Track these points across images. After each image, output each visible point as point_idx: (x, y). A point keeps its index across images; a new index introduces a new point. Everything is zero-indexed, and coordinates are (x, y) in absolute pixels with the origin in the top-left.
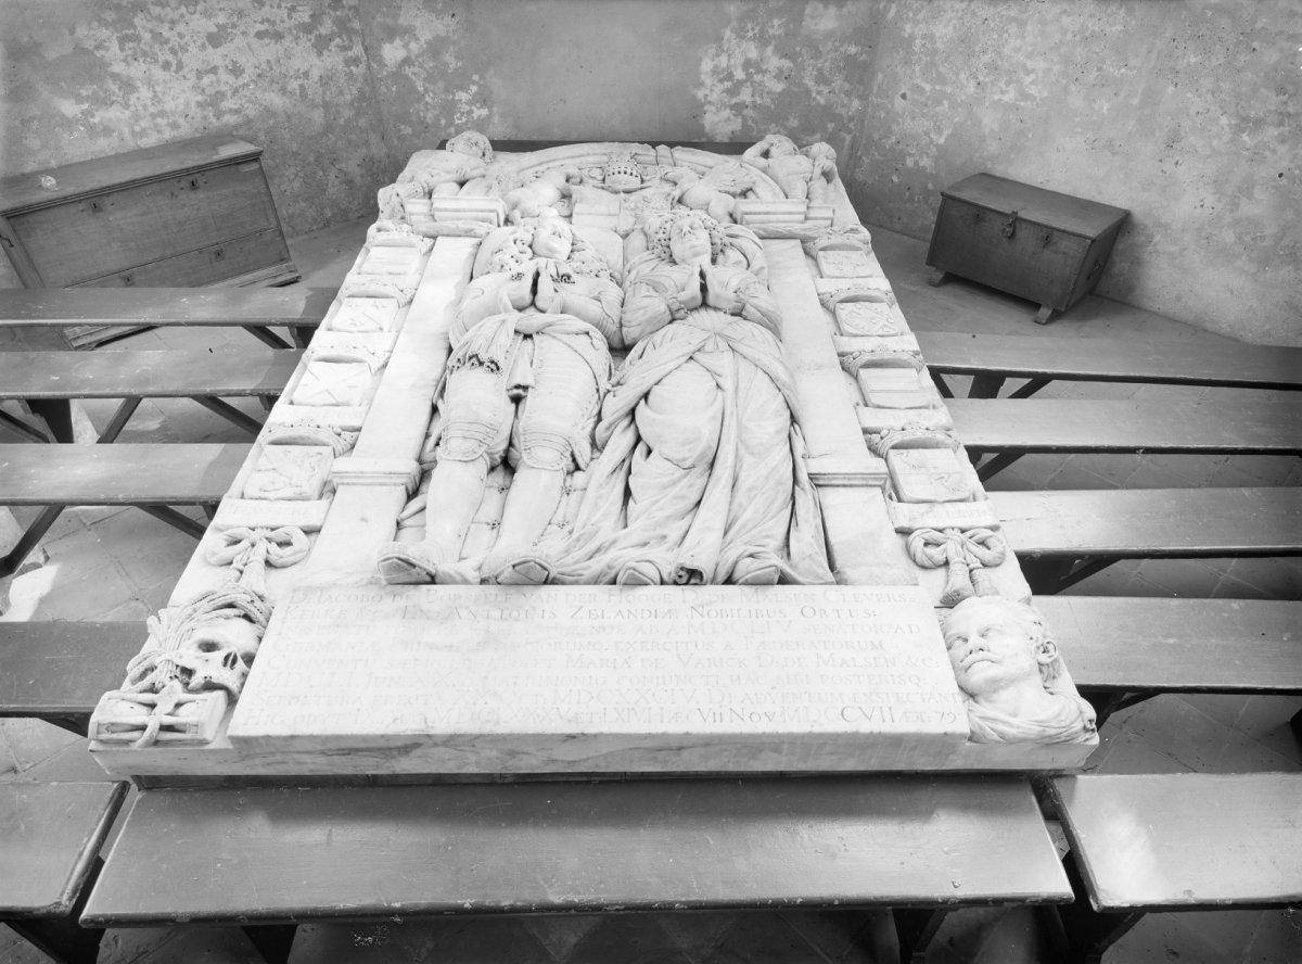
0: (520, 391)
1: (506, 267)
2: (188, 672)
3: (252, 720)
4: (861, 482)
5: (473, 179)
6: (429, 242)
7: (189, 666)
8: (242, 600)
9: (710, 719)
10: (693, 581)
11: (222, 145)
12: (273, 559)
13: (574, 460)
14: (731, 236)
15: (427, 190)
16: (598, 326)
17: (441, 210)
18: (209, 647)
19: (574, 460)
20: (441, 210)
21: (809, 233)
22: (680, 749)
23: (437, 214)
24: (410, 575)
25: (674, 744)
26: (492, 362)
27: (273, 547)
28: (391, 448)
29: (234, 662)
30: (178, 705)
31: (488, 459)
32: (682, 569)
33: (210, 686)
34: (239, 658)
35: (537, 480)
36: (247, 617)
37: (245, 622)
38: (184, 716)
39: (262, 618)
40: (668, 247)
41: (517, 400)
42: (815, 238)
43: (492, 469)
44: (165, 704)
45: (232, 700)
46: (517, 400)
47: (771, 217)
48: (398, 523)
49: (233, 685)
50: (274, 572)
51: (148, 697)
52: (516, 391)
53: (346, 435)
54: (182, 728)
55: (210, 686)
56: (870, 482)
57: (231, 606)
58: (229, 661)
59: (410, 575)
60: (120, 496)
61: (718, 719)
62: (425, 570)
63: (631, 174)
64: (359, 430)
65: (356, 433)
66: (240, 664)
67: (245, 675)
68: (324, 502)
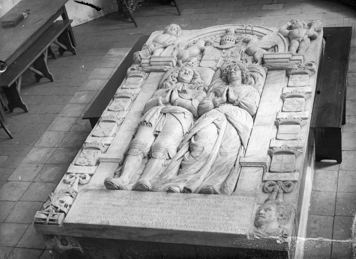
0: (157, 133)
2: (57, 208)
3: (70, 219)
4: (249, 165)
5: (169, 46)
7: (57, 206)
8: (71, 192)
9: (179, 227)
10: (188, 192)
11: (87, 23)
12: (81, 182)
13: (169, 156)
14: (252, 71)
15: (151, 52)
16: (189, 110)
17: (153, 62)
18: (62, 202)
19: (169, 156)
20: (153, 62)
21: (289, 67)
22: (172, 235)
23: (152, 63)
27: (81, 179)
28: (116, 152)
29: (67, 206)
30: (54, 215)
31: (142, 155)
34: (68, 206)
36: (71, 196)
37: (71, 198)
38: (56, 217)
39: (74, 197)
40: (227, 77)
41: (156, 136)
42: (291, 69)
43: (145, 157)
46: (156, 136)
47: (276, 60)
48: (115, 173)
50: (80, 186)
51: (47, 213)
52: (156, 133)
53: (106, 147)
54: (54, 220)
55: (61, 211)
56: (252, 165)
57: (68, 193)
61: (181, 227)
62: (116, 185)
63: (230, 40)
64: (109, 145)
65: (109, 146)
66: (68, 207)
68: (96, 167)
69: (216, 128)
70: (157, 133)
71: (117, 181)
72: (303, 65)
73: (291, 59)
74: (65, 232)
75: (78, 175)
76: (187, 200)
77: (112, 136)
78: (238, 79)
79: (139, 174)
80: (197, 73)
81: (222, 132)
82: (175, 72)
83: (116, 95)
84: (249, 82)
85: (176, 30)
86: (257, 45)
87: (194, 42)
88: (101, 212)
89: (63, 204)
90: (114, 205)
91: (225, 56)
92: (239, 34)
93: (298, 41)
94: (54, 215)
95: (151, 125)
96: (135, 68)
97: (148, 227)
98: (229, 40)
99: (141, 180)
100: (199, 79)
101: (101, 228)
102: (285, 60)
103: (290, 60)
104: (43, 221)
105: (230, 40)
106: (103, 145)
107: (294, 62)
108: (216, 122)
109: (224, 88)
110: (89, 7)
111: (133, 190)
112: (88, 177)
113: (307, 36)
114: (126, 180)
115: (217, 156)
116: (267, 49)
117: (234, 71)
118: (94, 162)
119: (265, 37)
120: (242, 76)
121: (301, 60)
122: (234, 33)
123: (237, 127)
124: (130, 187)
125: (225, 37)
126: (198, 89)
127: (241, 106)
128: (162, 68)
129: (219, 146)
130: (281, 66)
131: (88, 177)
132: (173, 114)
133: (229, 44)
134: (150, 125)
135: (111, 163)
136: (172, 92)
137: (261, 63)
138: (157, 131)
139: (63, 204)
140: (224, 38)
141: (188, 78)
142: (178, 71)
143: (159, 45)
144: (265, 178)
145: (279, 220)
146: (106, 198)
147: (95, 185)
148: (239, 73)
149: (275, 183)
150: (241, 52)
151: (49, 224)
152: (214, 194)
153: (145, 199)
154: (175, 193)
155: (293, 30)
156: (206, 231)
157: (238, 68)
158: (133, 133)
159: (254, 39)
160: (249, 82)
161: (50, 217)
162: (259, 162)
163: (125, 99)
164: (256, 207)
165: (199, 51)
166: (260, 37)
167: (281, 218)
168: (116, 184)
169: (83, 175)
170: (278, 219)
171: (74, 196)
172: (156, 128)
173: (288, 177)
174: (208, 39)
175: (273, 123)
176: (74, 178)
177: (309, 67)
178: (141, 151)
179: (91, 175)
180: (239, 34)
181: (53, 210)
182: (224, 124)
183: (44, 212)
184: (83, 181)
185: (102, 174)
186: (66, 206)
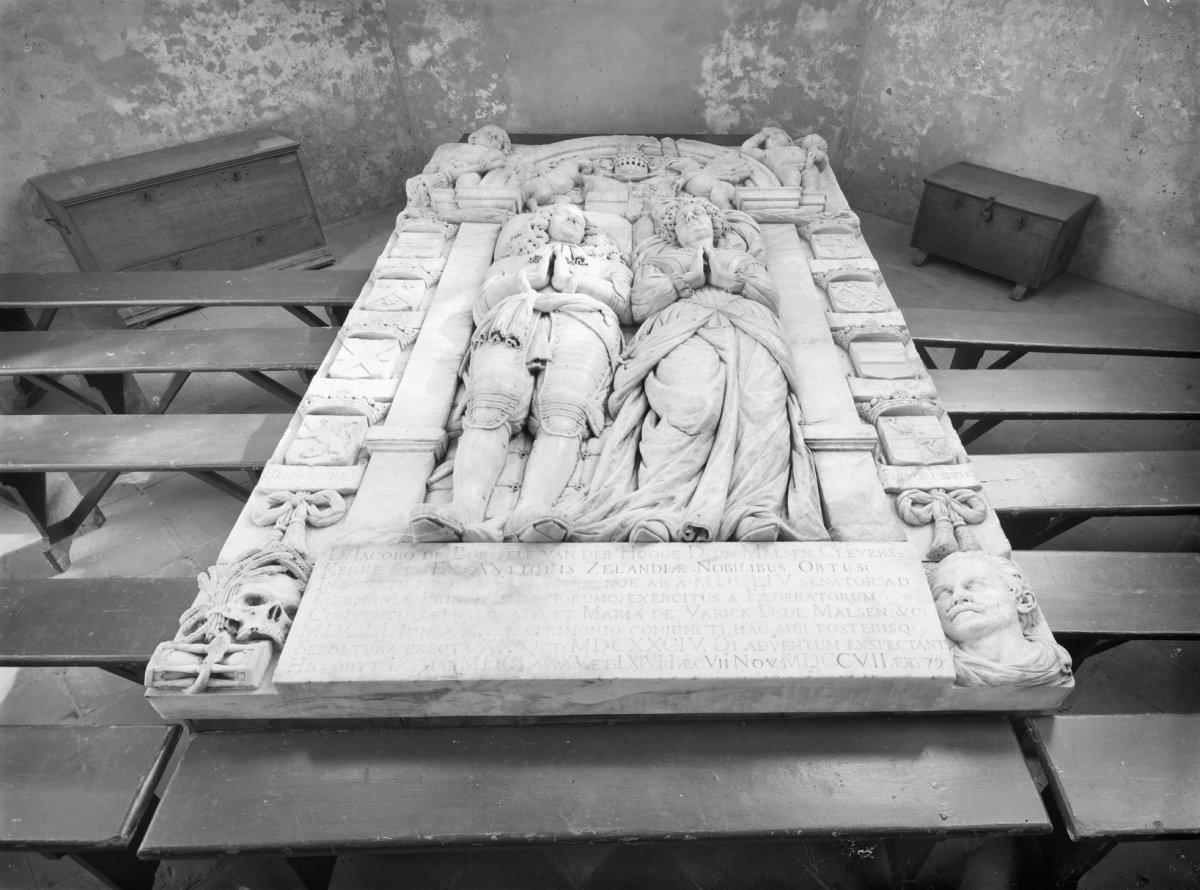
2: (236, 624)
3: (295, 667)
4: (852, 447)
5: (493, 169)
8: (285, 557)
10: (699, 538)
12: (313, 519)
22: (688, 693)
24: (439, 534)
25: (683, 688)
26: (513, 338)
27: (313, 509)
29: (279, 614)
30: (227, 654)
31: (510, 428)
33: (256, 637)
34: (283, 612)
35: (554, 448)
36: (290, 574)
38: (234, 664)
39: (303, 574)
41: (536, 373)
43: (513, 437)
44: (215, 654)
45: (277, 649)
48: (428, 487)
50: (314, 532)
51: (199, 647)
52: (534, 365)
53: (379, 406)
55: (256, 637)
57: (275, 563)
59: (439, 534)
61: (724, 665)
65: (387, 405)
66: (284, 616)
67: (288, 627)
68: (359, 468)
76: (706, 564)
79: (510, 487)
88: (416, 629)
90: (459, 600)
91: (640, 194)
95: (518, 344)
105: (639, 164)
106: (373, 402)
110: (96, 670)
120: (714, 228)
126: (608, 258)
130: (785, 216)
131: (338, 503)
132: (571, 313)
134: (513, 342)
135: (409, 454)
138: (537, 360)
139: (264, 609)
145: (1024, 618)
147: (371, 529)
153: (566, 569)
154: (659, 544)
161: (212, 664)
162: (859, 437)
168: (451, 525)
170: (1020, 613)
171: (299, 571)
178: (506, 417)
179: (348, 494)
181: (225, 633)
186: (274, 614)
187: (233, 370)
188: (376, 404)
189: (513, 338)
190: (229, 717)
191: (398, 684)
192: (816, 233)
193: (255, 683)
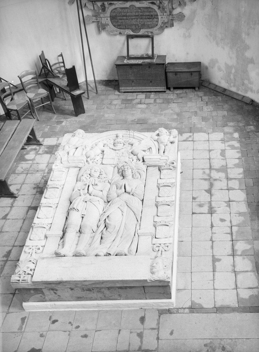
1: (84, 181)
3: (36, 278)
6: (67, 169)
18: (28, 268)
24: (58, 255)
25: (102, 282)
26: (78, 209)
27: (37, 250)
29: (32, 270)
30: (24, 277)
32: (107, 253)
33: (28, 274)
35: (87, 236)
36: (33, 263)
38: (25, 278)
40: (122, 173)
41: (83, 217)
44: (22, 277)
45: (32, 276)
47: (151, 160)
49: (32, 274)
51: (19, 276)
55: (28, 274)
57: (30, 261)
58: (31, 270)
59: (58, 255)
60: (212, 268)
66: (33, 271)
67: (34, 273)
69: (121, 212)
70: (83, 216)
71: (62, 252)
72: (168, 163)
73: (161, 159)
74: (33, 286)
75: (34, 248)
77: (51, 218)
78: (130, 175)
80: (102, 170)
81: (125, 214)
82: (87, 170)
83: (48, 185)
84: (136, 177)
85: (82, 134)
86: (138, 148)
87: (95, 144)
89: (29, 269)
92: (125, 137)
93: (164, 145)
94: (24, 277)
96: (58, 164)
97: (88, 280)
98: (120, 143)
99: (78, 249)
100: (104, 175)
101: (57, 282)
102: (157, 160)
103: (160, 160)
104: (18, 281)
107: (163, 161)
108: (121, 208)
109: (122, 182)
111: (73, 256)
112: (41, 248)
113: (169, 142)
114: (68, 249)
115: (124, 230)
116: (144, 151)
117: (127, 170)
118: (43, 237)
119: (143, 142)
121: (167, 160)
122: (122, 137)
123: (133, 211)
124: (71, 254)
125: (116, 141)
127: (134, 195)
128: (77, 165)
129: (124, 224)
131: (41, 248)
133: (119, 146)
134: (78, 210)
136: (89, 186)
137: (142, 161)
140: (116, 141)
141: (97, 174)
142: (90, 169)
143: (51, 75)
144: (154, 243)
146: (57, 263)
148: (130, 171)
149: (160, 245)
150: (128, 153)
151: (21, 282)
152: (125, 255)
155: (160, 137)
156: (123, 279)
157: (129, 168)
158: (66, 215)
159: (135, 142)
160: (136, 177)
163: (55, 189)
164: (150, 261)
165: (101, 151)
166: (140, 141)
167: (165, 267)
169: (37, 247)
172: (82, 213)
173: (167, 241)
174: (105, 142)
175: (154, 205)
176: (31, 249)
177: (172, 165)
180: (125, 137)
182: (125, 209)
183: (17, 276)
184: (39, 251)
185: (52, 246)
186: (31, 270)
187: (9, 212)
188: (48, 225)
189: (78, 209)
190: (109, 71)
191: (53, 281)
192: (162, 170)
193: (29, 282)
